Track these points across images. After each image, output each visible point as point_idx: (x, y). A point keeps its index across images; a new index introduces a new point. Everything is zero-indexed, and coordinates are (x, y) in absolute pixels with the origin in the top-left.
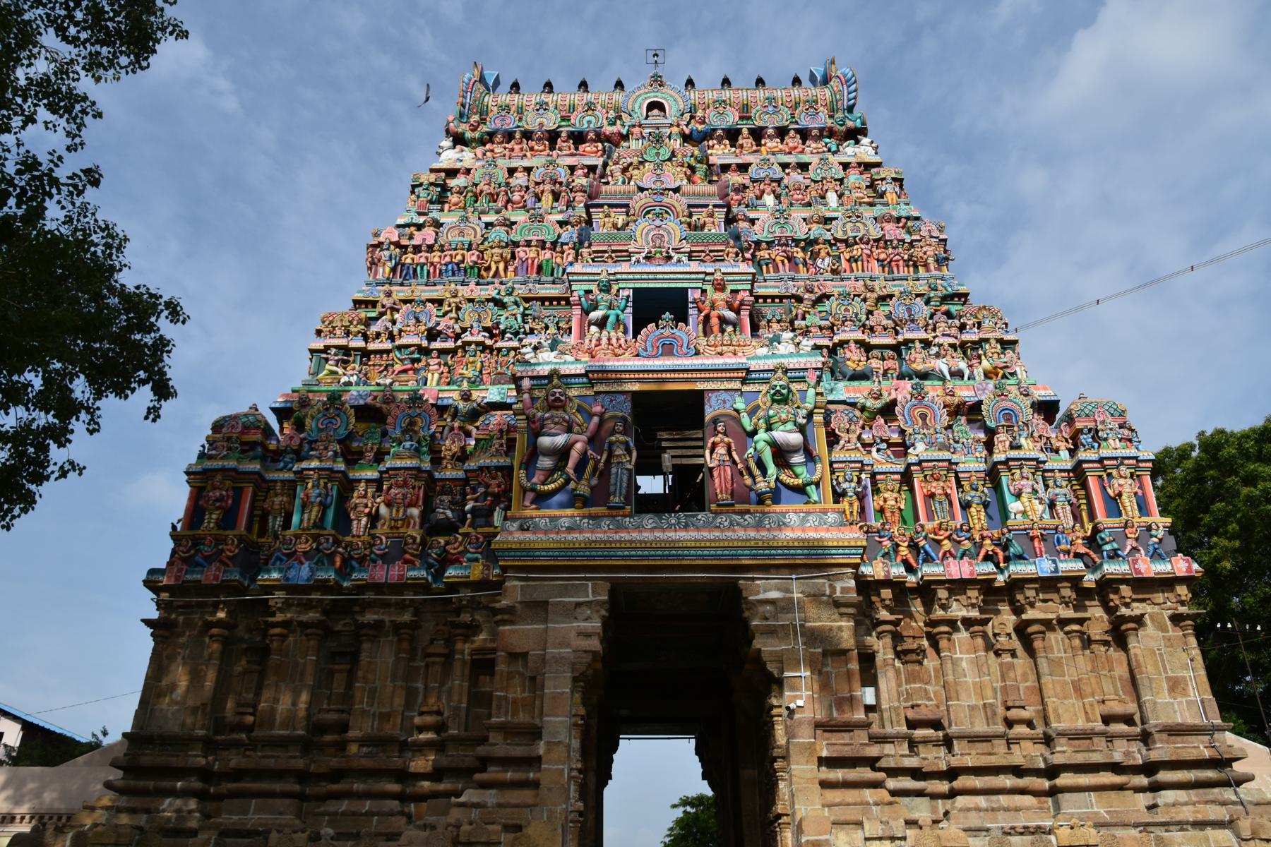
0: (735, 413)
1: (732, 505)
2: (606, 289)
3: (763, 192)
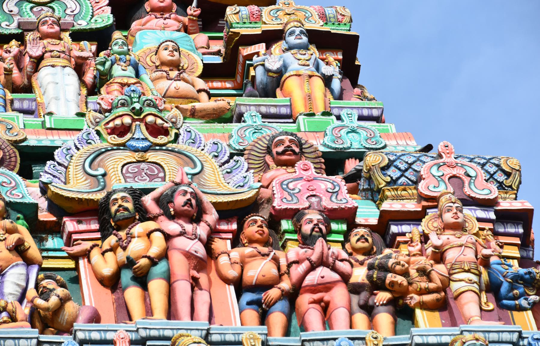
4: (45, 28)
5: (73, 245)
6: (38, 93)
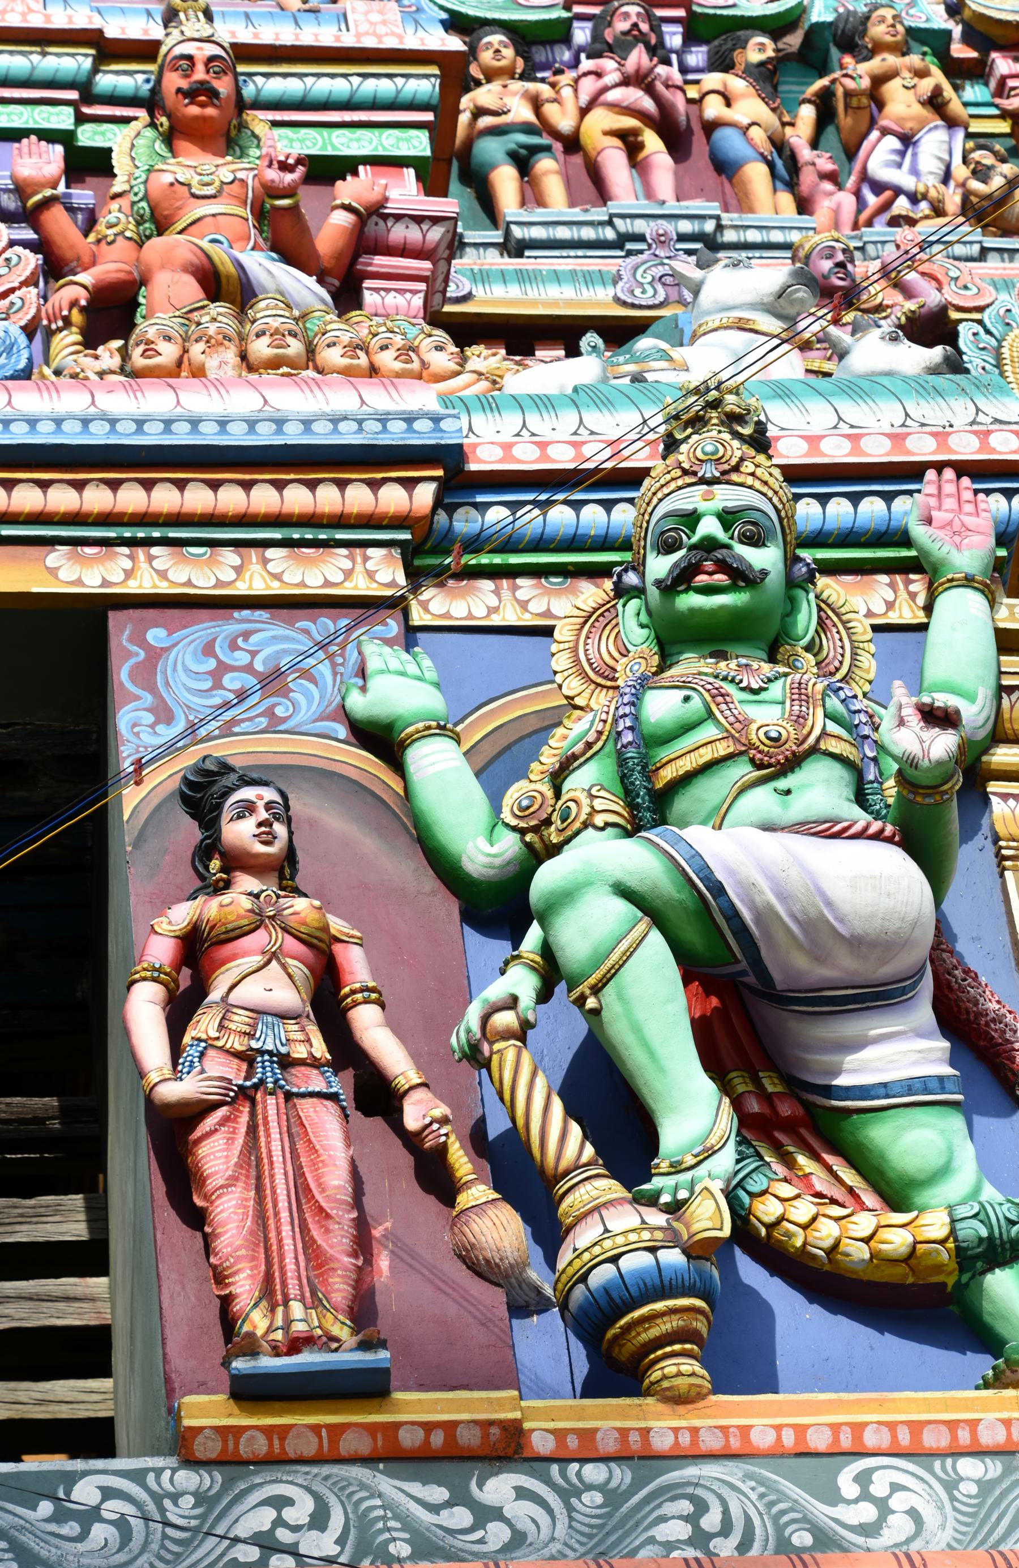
0: (362, 762)
1: (369, 1387)
5: (1008, 97)
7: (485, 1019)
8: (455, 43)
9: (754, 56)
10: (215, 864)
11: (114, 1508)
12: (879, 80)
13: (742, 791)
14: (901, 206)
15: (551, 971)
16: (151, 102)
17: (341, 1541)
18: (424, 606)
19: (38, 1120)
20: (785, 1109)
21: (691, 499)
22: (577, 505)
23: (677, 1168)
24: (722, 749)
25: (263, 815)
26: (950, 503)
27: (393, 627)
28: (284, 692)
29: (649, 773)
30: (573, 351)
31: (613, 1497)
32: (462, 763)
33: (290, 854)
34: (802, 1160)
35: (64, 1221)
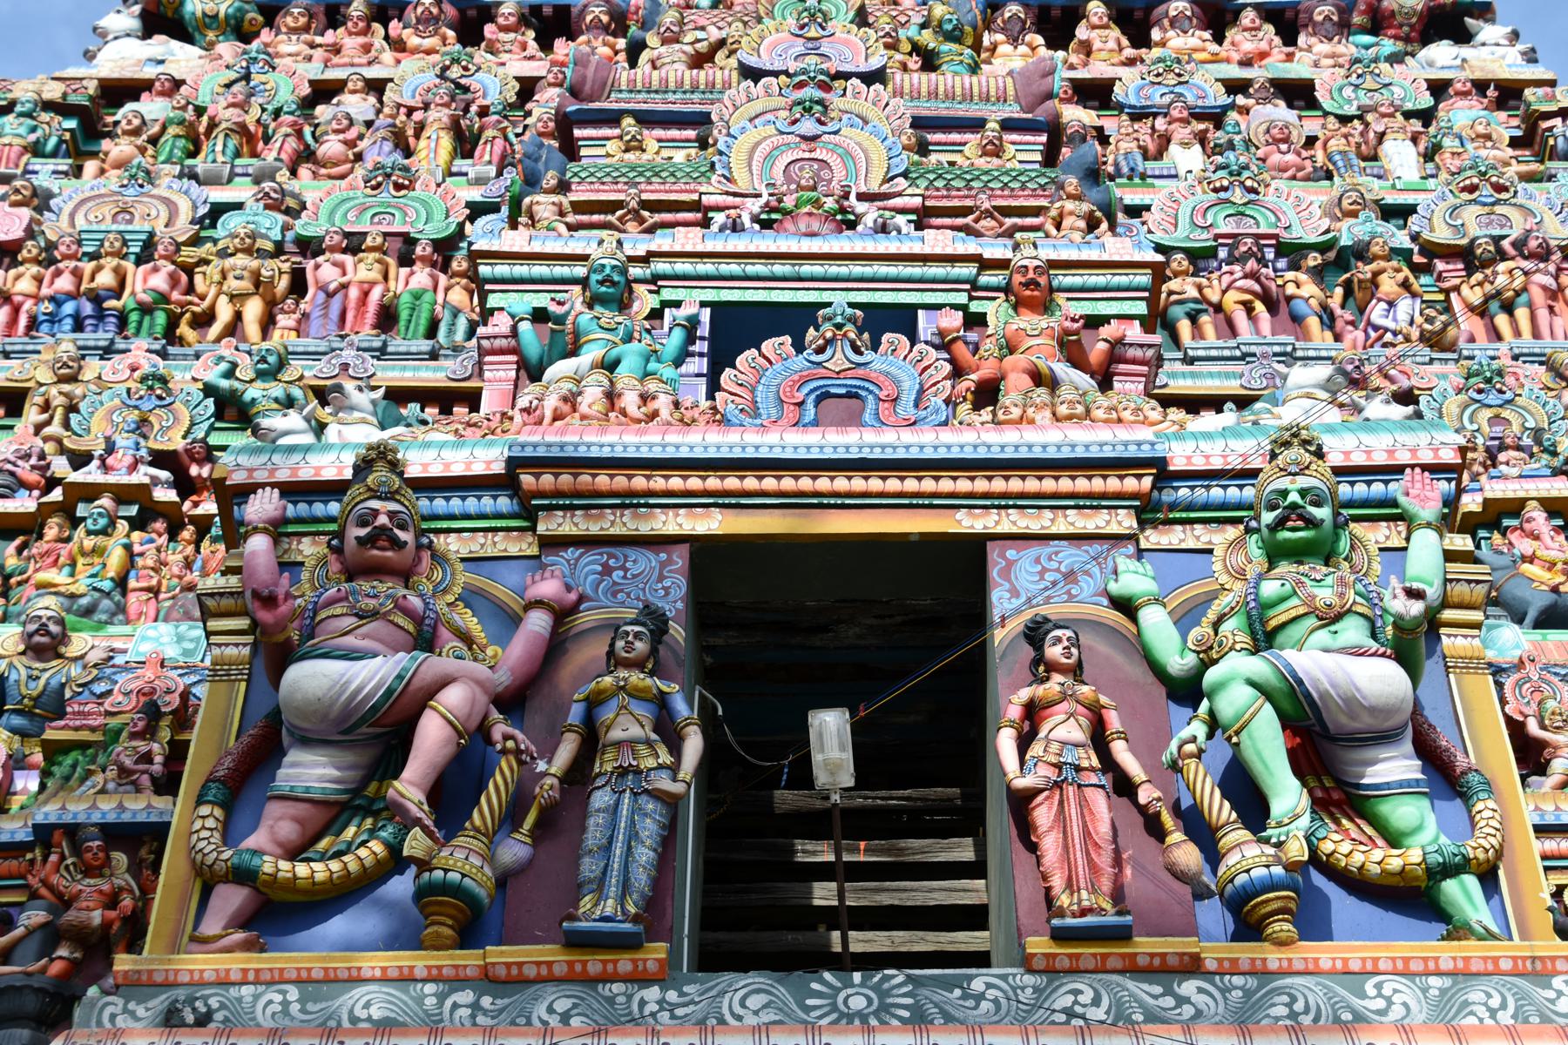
1: (1121, 935)
2: (613, 293)
3: (1165, 140)
4: (1383, 109)
6: (1384, 161)
7: (1180, 748)
8: (1160, 258)
9: (1311, 263)
10: (1041, 668)
11: (991, 993)
12: (1376, 274)
13: (1312, 631)
14: (1388, 337)
15: (1213, 724)
16: (1007, 289)
17: (1107, 1013)
18: (1147, 538)
19: (950, 800)
20: (1335, 796)
21: (1284, 483)
22: (1225, 487)
23: (1280, 825)
24: (1301, 611)
25: (1066, 644)
26: (1418, 485)
27: (1131, 549)
28: (1076, 582)
29: (1264, 623)
30: (1219, 410)
31: (1248, 993)
32: (1167, 617)
33: (1080, 663)
34: (1344, 821)
35: (964, 851)
